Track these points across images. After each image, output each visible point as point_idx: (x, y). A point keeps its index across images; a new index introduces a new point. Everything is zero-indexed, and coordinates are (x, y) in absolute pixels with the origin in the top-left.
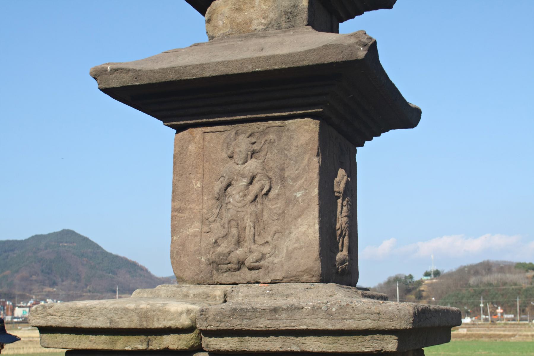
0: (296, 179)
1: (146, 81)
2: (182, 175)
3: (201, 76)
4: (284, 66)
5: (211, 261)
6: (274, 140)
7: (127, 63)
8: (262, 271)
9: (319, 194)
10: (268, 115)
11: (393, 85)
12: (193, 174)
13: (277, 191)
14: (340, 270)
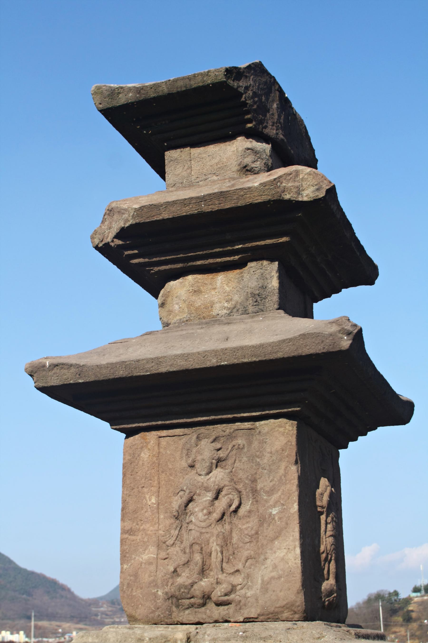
0: (270, 492)
1: (92, 378)
2: (133, 489)
3: (156, 372)
4: (254, 359)
5: (170, 595)
6: (244, 445)
7: (69, 357)
8: (232, 606)
9: (300, 510)
10: (235, 415)
11: (382, 376)
12: (147, 487)
13: (248, 508)
14: (327, 603)
